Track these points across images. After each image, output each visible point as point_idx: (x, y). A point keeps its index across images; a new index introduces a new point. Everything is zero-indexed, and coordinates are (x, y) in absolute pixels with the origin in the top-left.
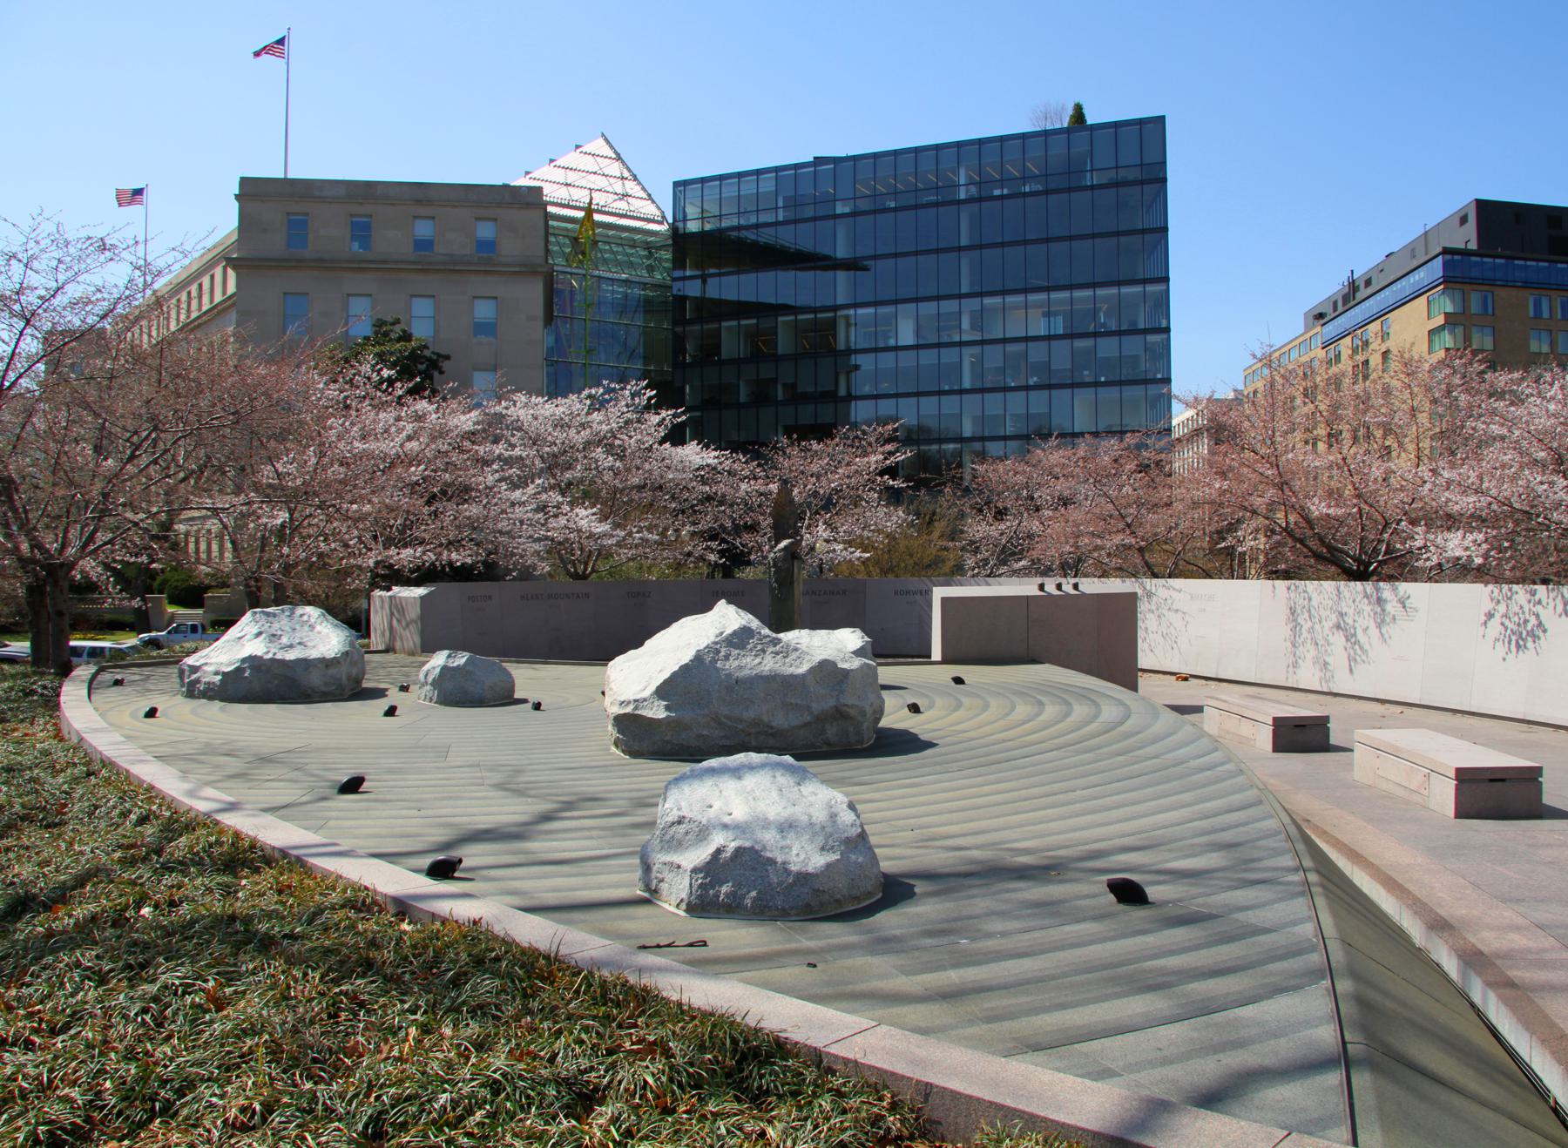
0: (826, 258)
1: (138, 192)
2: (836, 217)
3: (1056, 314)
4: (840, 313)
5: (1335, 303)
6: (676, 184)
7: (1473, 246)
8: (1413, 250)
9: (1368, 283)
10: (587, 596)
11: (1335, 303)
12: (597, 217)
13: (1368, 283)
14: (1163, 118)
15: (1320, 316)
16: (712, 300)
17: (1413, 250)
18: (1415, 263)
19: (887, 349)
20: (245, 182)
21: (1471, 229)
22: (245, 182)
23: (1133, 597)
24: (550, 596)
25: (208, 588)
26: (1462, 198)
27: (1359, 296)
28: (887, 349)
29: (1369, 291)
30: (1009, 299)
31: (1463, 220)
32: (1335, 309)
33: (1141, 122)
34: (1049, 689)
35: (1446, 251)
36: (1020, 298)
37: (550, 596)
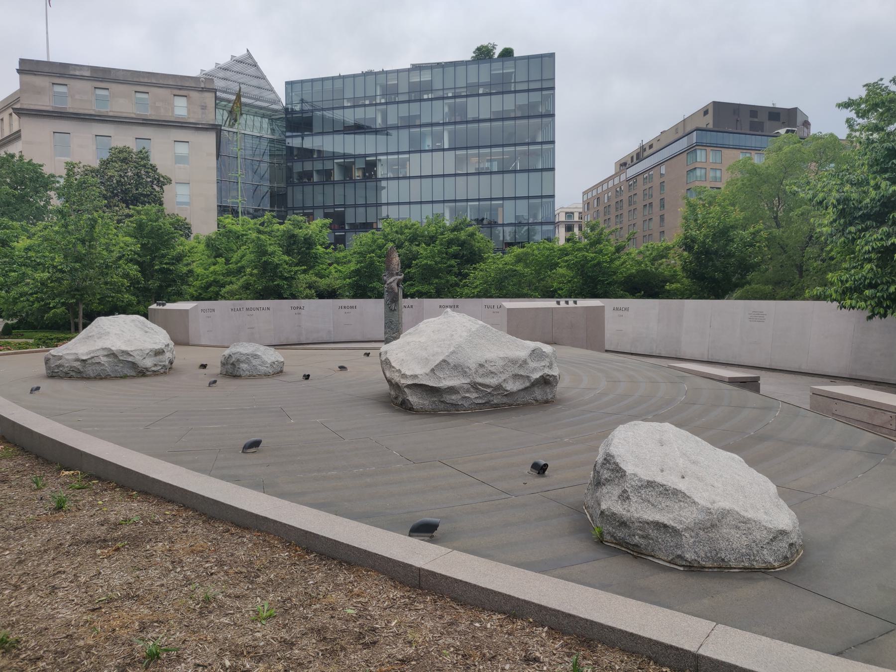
0: (368, 127)
1: (256, 444)
3: (495, 160)
4: (379, 158)
5: (632, 158)
7: (711, 126)
8: (677, 129)
9: (651, 147)
10: (268, 309)
11: (632, 158)
14: (552, 56)
15: (625, 164)
16: (306, 150)
18: (677, 136)
19: (405, 178)
20: (22, 61)
22: (22, 61)
23: (601, 309)
25: (665, 281)
27: (646, 154)
28: (405, 178)
29: (652, 151)
30: (470, 152)
31: (706, 112)
32: (632, 161)
33: (541, 56)
35: (697, 129)
36: (476, 151)
37: (247, 309)
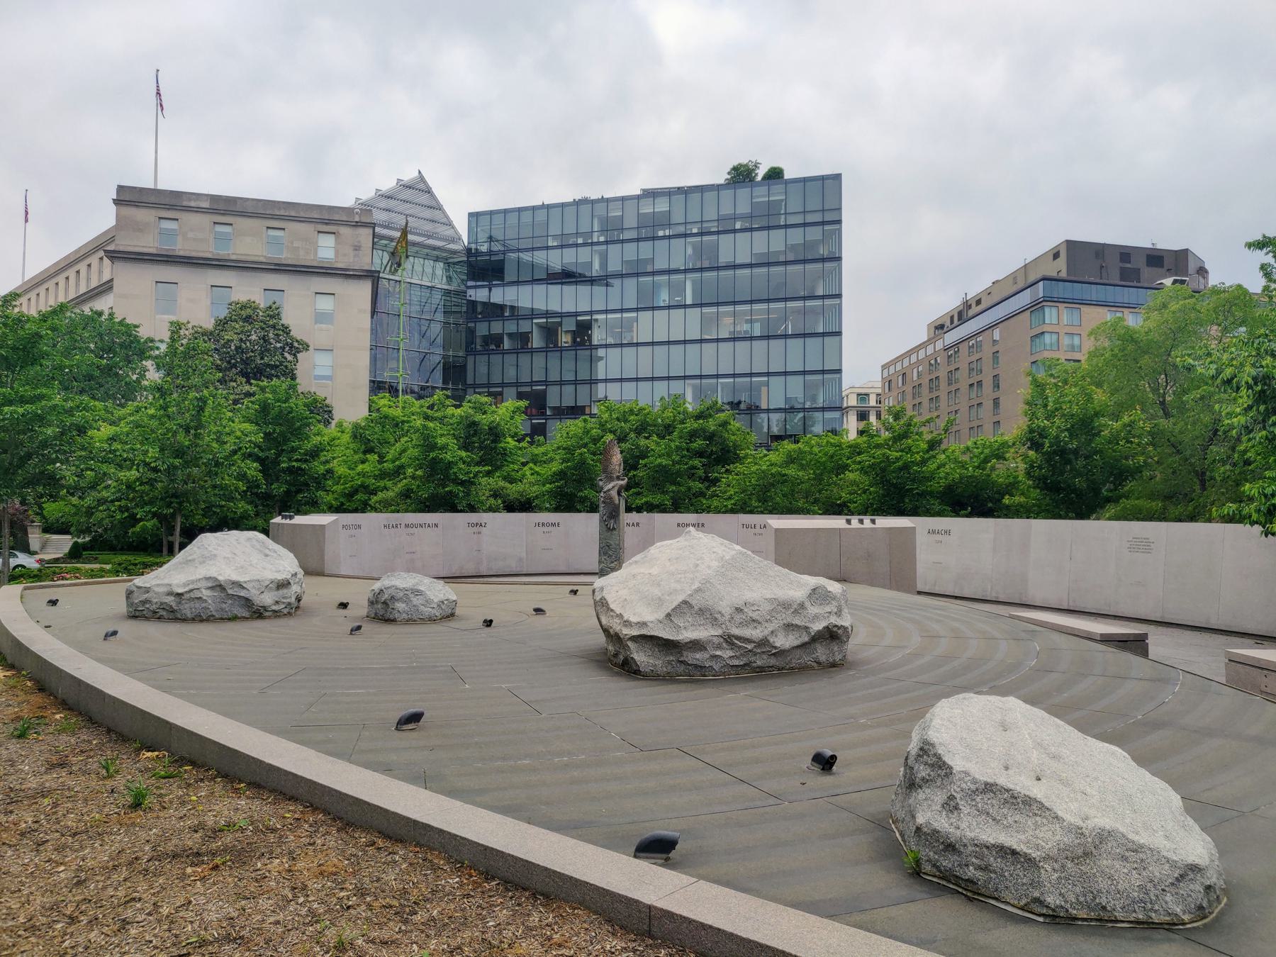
1: (415, 718)
2: (547, 248)
3: (757, 320)
4: (595, 317)
5: (952, 318)
6: (471, 215)
7: (1064, 274)
9: (979, 302)
10: (436, 525)
11: (952, 318)
12: (410, 237)
13: (979, 302)
15: (942, 327)
17: (1015, 278)
18: (1015, 289)
21: (1062, 264)
24: (407, 526)
26: (1054, 239)
27: (971, 313)
30: (722, 309)
31: (1056, 256)
32: (952, 322)
34: (1058, 726)
36: (730, 308)
37: (407, 526)
